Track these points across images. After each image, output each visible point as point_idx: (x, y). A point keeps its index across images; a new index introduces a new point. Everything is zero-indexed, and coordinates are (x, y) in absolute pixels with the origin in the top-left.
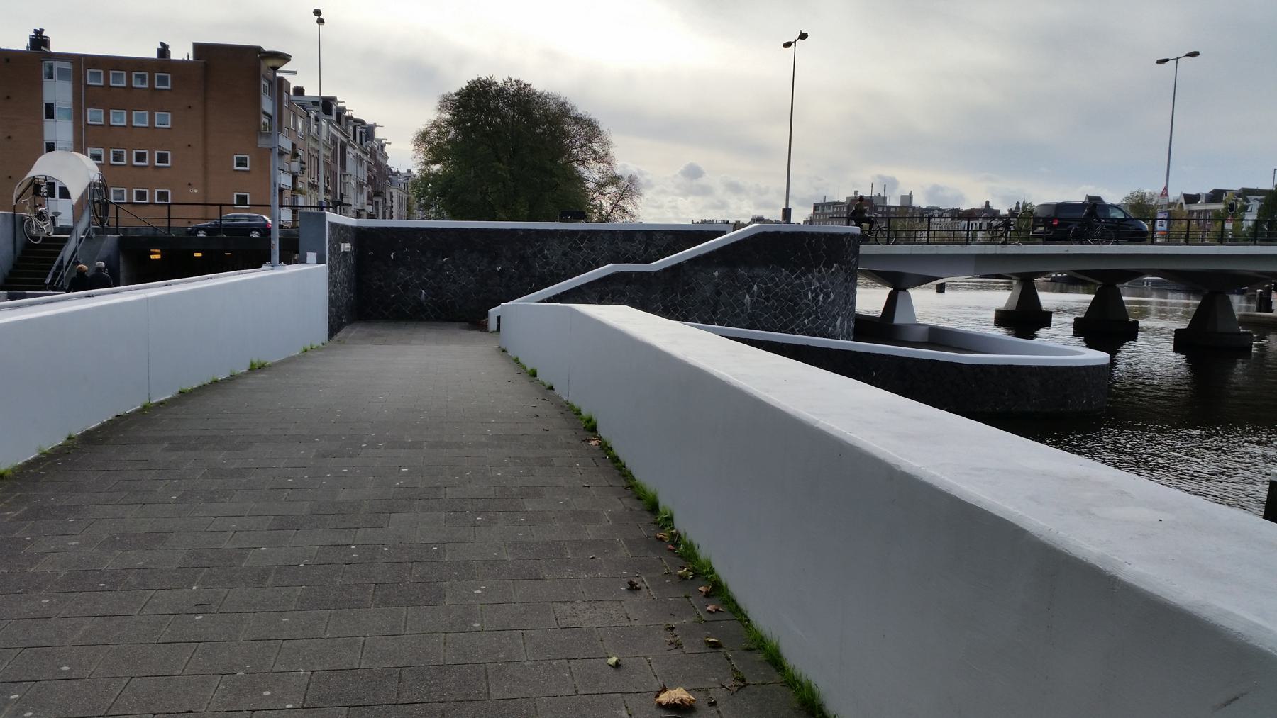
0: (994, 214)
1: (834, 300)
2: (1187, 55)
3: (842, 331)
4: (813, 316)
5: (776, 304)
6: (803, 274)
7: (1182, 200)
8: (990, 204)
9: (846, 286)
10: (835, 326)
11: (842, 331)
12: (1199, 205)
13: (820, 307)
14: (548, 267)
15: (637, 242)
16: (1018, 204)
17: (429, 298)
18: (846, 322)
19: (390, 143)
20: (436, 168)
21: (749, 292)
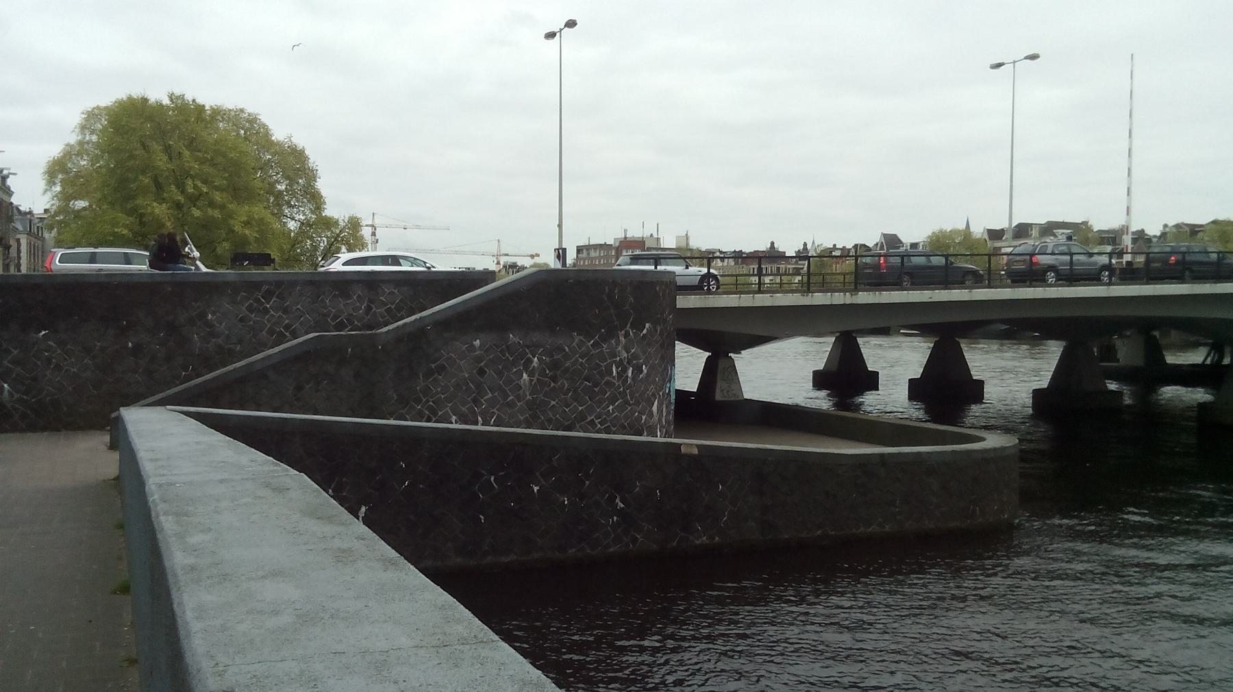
0: (782, 257)
1: (648, 375)
2: (1026, 58)
3: (660, 420)
4: (620, 401)
5: (566, 385)
6: (604, 339)
7: (986, 236)
8: (776, 246)
9: (662, 356)
10: (651, 413)
11: (660, 420)
12: (1004, 241)
13: (630, 387)
14: (214, 340)
15: (355, 298)
16: (805, 244)
17: (16, 396)
18: (664, 405)
19: (15, 174)
20: (81, 204)
21: (526, 368)
